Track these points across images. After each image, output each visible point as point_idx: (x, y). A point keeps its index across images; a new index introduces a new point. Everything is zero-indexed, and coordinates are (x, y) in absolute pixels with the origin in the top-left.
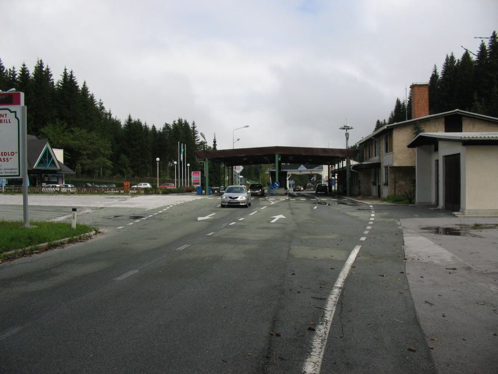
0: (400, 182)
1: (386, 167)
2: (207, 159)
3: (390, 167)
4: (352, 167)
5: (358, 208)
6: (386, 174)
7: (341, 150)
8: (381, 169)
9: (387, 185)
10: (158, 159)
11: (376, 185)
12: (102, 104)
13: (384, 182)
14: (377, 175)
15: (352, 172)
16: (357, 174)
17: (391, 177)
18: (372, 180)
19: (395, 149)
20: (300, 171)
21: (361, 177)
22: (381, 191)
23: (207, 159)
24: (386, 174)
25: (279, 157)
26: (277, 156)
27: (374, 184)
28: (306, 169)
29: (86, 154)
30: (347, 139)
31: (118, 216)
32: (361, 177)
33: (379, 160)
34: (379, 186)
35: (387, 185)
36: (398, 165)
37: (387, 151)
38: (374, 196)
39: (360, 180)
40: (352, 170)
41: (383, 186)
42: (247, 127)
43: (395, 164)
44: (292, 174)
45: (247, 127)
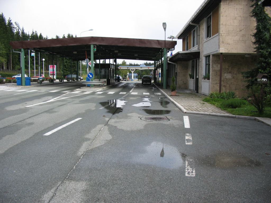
0: (225, 75)
1: (208, 57)
2: (22, 50)
3: (213, 55)
4: (168, 59)
5: (171, 94)
6: (208, 65)
7: (158, 41)
8: (200, 60)
9: (209, 79)
10: (44, 60)
11: (193, 78)
12: (11, 20)
13: (204, 74)
14: (195, 67)
15: (168, 63)
16: (175, 65)
17: (215, 67)
18: (190, 72)
19: (222, 29)
20: (141, 67)
21: (178, 69)
22: (199, 85)
23: (22, 50)
24: (206, 64)
25: (94, 47)
26: (92, 46)
27: (192, 77)
28: (145, 66)
29: (254, 80)
30: (165, 29)
31: (199, 66)
32: (178, 69)
33: (198, 48)
34: (197, 80)
35: (209, 79)
36: (226, 52)
37: (208, 35)
38: (190, 90)
39: (177, 73)
40: (168, 62)
41: (203, 80)
42: (91, 30)
43: (223, 50)
44: (136, 69)
45: (91, 30)
